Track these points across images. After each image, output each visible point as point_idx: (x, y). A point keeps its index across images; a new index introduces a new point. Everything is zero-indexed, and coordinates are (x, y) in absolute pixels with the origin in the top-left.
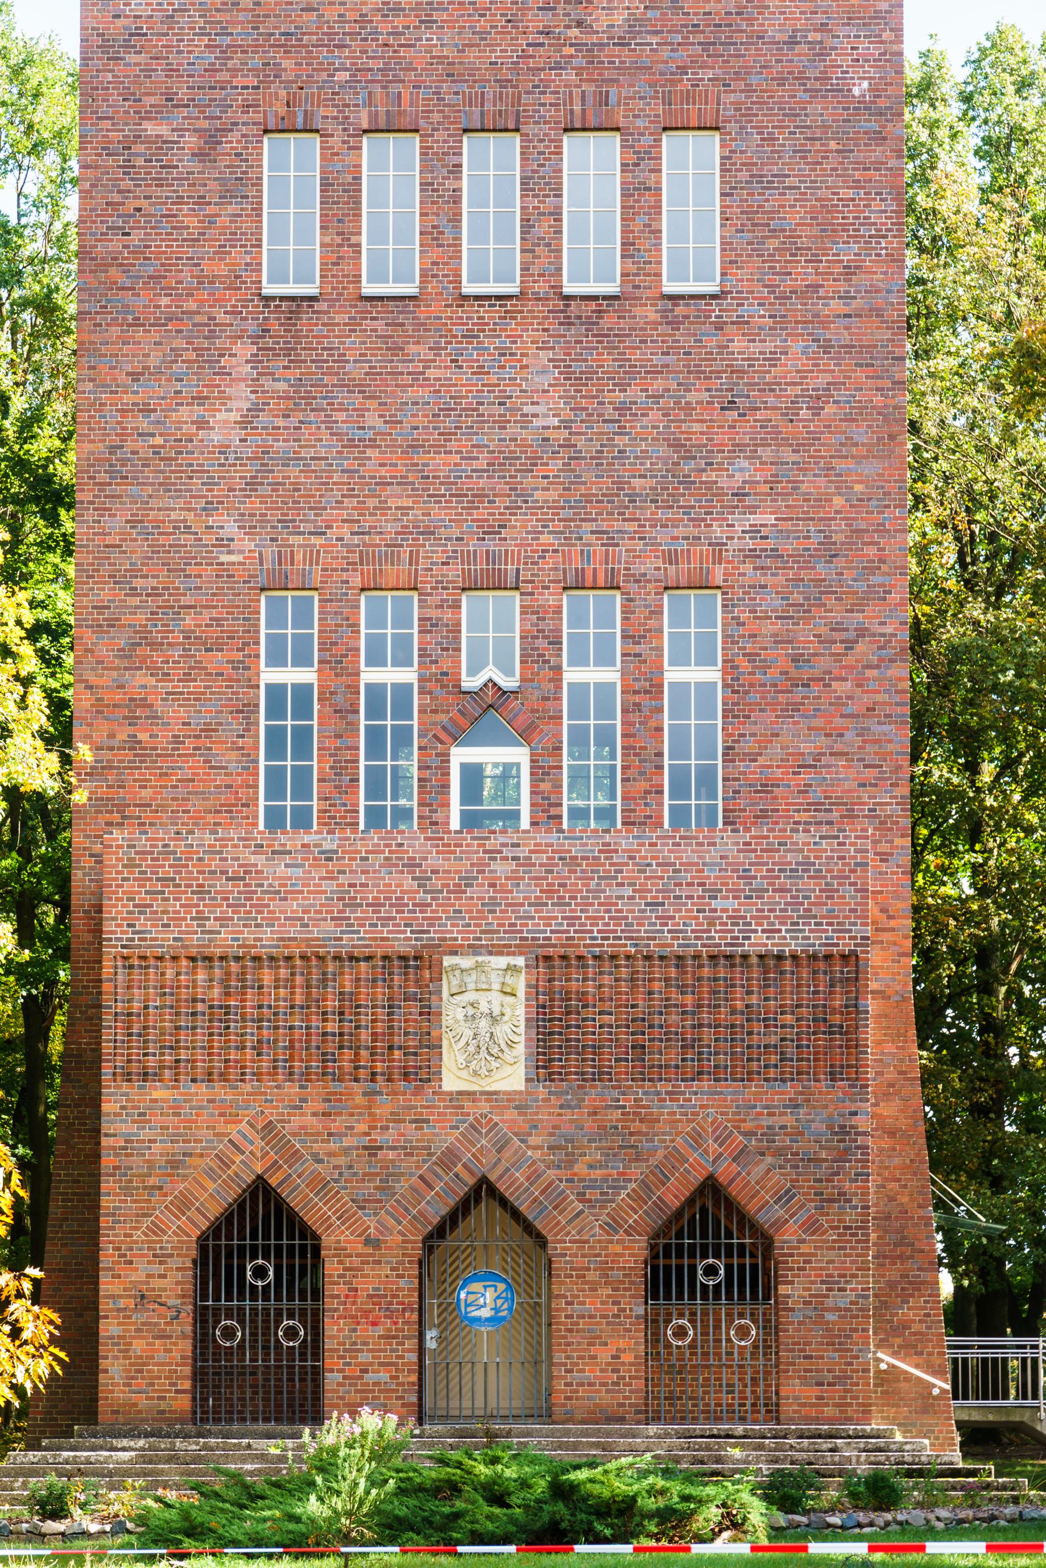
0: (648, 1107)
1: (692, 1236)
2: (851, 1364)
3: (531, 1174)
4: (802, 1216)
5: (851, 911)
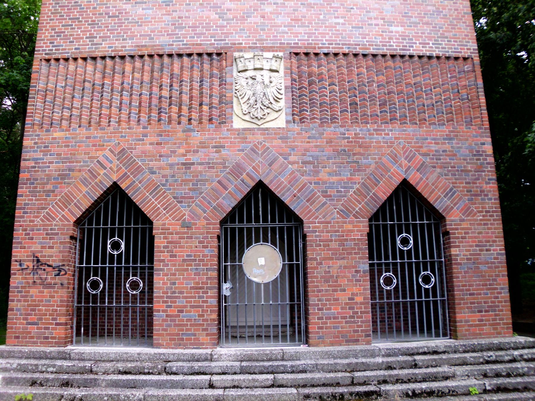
0: (364, 138)
1: (392, 219)
2: (497, 298)
3: (292, 179)
4: (461, 205)
5: (465, 35)
